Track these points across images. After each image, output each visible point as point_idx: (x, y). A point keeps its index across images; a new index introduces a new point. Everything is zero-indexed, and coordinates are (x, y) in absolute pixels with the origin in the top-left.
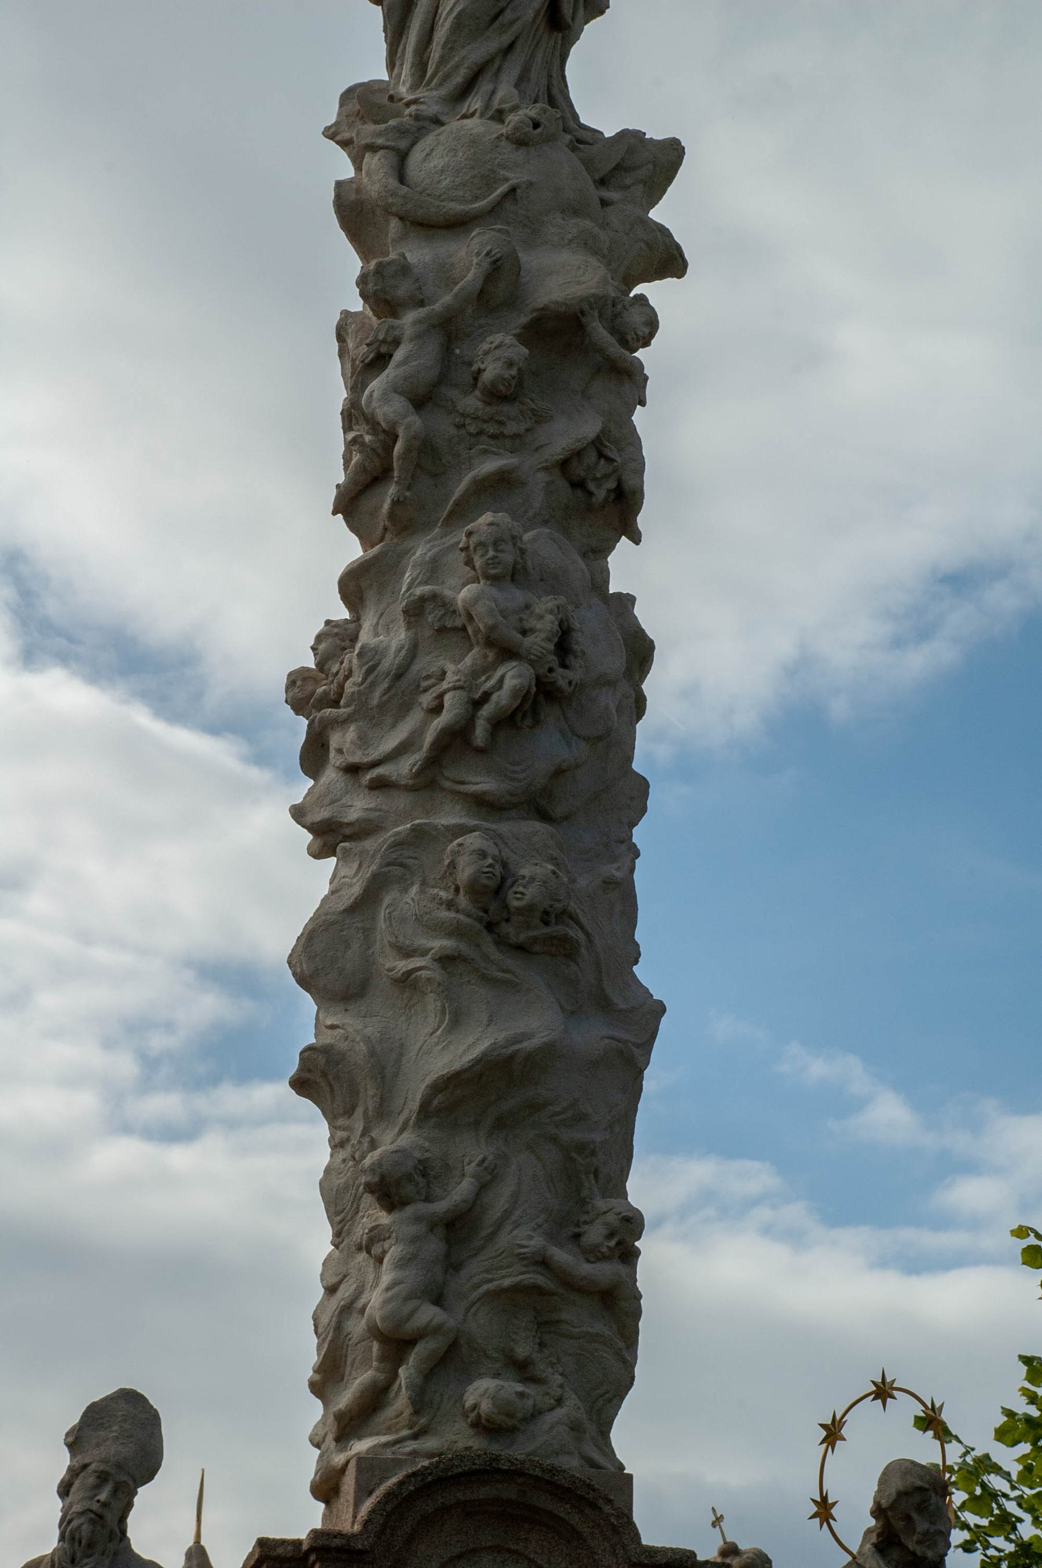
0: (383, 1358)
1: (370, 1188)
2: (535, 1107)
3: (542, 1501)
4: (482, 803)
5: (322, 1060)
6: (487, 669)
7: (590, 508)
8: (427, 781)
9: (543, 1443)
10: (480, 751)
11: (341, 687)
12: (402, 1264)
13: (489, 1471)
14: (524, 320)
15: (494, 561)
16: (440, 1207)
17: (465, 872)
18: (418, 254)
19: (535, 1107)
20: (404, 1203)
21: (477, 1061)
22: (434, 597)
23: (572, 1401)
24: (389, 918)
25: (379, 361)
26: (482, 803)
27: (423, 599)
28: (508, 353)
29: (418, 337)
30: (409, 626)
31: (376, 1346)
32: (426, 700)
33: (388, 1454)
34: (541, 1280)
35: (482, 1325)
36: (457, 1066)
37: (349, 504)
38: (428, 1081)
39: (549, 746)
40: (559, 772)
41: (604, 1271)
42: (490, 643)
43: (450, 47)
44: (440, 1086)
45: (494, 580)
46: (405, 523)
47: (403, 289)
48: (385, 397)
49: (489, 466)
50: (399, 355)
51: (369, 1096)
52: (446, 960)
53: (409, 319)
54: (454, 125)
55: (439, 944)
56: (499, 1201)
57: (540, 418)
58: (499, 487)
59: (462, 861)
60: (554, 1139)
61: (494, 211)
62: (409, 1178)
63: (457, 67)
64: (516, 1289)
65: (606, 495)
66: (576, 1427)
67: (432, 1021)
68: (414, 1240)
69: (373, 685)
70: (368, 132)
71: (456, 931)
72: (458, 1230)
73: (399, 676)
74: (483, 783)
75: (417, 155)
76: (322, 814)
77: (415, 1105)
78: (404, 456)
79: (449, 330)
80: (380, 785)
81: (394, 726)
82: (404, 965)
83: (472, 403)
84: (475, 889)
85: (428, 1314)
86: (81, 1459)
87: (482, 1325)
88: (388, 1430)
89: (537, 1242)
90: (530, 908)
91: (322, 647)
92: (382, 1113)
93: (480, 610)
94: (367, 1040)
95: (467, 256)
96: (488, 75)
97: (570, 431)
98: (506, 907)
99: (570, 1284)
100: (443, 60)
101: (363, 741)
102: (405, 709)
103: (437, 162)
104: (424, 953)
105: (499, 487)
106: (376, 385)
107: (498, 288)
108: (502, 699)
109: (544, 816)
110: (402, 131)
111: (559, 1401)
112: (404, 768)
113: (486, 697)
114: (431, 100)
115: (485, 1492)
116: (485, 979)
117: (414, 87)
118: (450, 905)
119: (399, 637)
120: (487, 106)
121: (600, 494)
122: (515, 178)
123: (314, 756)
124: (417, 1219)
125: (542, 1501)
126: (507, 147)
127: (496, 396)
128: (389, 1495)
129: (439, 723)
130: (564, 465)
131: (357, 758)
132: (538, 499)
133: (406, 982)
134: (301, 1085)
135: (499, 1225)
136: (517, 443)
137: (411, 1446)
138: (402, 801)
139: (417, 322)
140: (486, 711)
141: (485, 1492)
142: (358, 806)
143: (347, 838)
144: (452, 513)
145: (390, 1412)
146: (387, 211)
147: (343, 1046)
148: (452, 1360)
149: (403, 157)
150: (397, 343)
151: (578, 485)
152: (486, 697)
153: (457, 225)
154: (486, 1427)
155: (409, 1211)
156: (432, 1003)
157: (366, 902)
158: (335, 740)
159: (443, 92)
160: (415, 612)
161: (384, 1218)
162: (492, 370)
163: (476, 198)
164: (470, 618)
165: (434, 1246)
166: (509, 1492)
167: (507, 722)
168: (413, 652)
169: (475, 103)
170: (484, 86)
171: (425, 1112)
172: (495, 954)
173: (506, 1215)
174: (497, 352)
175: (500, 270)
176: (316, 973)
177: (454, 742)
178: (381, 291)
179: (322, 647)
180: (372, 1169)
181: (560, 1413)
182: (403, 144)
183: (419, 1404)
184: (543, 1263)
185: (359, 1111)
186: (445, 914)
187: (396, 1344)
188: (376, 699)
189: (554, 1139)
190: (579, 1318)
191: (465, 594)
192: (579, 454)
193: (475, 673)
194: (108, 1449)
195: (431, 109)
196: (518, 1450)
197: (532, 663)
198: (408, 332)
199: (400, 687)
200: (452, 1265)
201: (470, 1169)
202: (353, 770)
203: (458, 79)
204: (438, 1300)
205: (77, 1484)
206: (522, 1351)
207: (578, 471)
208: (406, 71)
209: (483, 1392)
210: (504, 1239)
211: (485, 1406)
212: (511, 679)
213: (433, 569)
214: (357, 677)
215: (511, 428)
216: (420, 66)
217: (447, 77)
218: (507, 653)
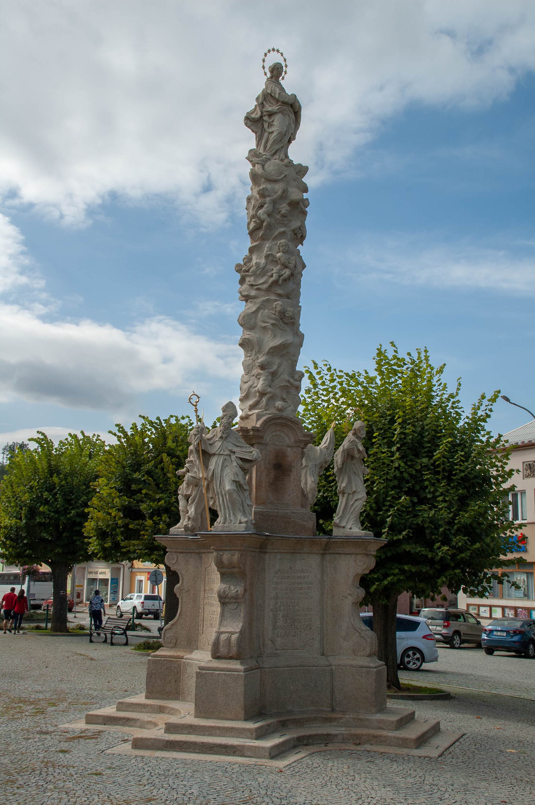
0: (259, 396)
1: (259, 366)
2: (288, 353)
3: (289, 423)
4: (280, 295)
5: (247, 341)
6: (282, 270)
7: (297, 239)
8: (269, 290)
9: (287, 413)
10: (279, 285)
11: (249, 269)
12: (264, 380)
13: (281, 418)
14: (288, 202)
15: (283, 249)
16: (272, 370)
17: (279, 308)
18: (269, 186)
19: (288, 353)
20: (265, 369)
21: (280, 344)
22: (271, 254)
23: (292, 406)
24: (261, 315)
25: (261, 207)
26: (280, 295)
27: (269, 254)
28: (287, 208)
29: (270, 203)
30: (265, 259)
31: (258, 394)
32: (269, 274)
33: (261, 413)
34: (288, 385)
35: (278, 392)
36: (275, 345)
37: (252, 233)
38: (269, 347)
39: (291, 285)
40: (293, 290)
41: (296, 383)
42: (283, 265)
43: (272, 145)
44: (271, 348)
45: (284, 252)
46: (264, 238)
47: (267, 193)
48: (263, 214)
49: (282, 230)
50: (266, 206)
51: (256, 349)
52: (273, 325)
53: (268, 199)
54: (273, 161)
55: (272, 321)
56: (281, 370)
57: (290, 221)
58: (282, 234)
59: (278, 306)
60: (290, 359)
61: (282, 179)
62: (266, 365)
63: (273, 149)
64: (284, 386)
65: (299, 236)
66: (293, 411)
67: (269, 336)
68: (267, 376)
69: (258, 270)
70: (255, 159)
71: (275, 319)
72: (274, 375)
73: (263, 269)
74: (280, 292)
75: (266, 166)
76: (246, 293)
77: (267, 351)
78: (265, 226)
79: (274, 202)
80: (258, 289)
81: (261, 278)
82: (264, 325)
83: (278, 217)
84: (280, 312)
85: (269, 390)
86: (225, 414)
87: (278, 392)
88: (260, 409)
89: (288, 378)
90: (290, 316)
91: (245, 260)
92: (259, 352)
93: (283, 258)
94: (256, 338)
95: (279, 187)
96: (279, 151)
97: (295, 224)
98: (285, 315)
99: (292, 385)
100: (270, 148)
101: (255, 280)
102: (264, 275)
103: (271, 168)
104: (268, 323)
105: (282, 234)
106: (261, 211)
107: (284, 195)
108: (285, 276)
109: (288, 298)
110: (263, 160)
111: (290, 406)
112: (265, 286)
113: (282, 275)
114: (268, 154)
115: (279, 421)
116: (280, 329)
117: (264, 151)
118: (274, 314)
119: (263, 261)
120: (279, 158)
121: (299, 237)
122: (286, 173)
123: (242, 281)
124: (268, 372)
125: (289, 423)
126: (284, 167)
127: (283, 216)
128: (265, 421)
129: (271, 280)
130: (293, 230)
131: (254, 283)
132: (289, 237)
133: (265, 328)
134: (241, 345)
135: (281, 374)
136: (286, 225)
137: (265, 412)
138: (262, 293)
139: (270, 200)
140: (282, 278)
141: (279, 421)
142: (253, 293)
143: (251, 298)
144: (274, 238)
145: (260, 406)
146: (262, 177)
147: (251, 338)
148: (273, 398)
149: (263, 166)
150: (265, 203)
151: (295, 234)
152: (282, 275)
153: (275, 181)
154: (280, 410)
155: (266, 371)
156: (270, 332)
157: (256, 312)
158: (248, 279)
159: (270, 153)
160: (267, 257)
161: (260, 371)
162: (283, 211)
163: (279, 176)
164: (280, 259)
165: (270, 377)
166: (283, 421)
167: (285, 280)
168: (266, 264)
169: (277, 157)
170: (278, 153)
171: (268, 353)
172: (282, 323)
173: (283, 372)
174: (284, 208)
175: (285, 191)
176: (245, 324)
177: (276, 282)
178: (263, 194)
179: (245, 260)
180: (260, 363)
181: (290, 408)
182: (263, 163)
183: (267, 405)
184: (289, 382)
185: (254, 351)
186: (273, 316)
187: (262, 394)
188: (258, 272)
189: (290, 359)
190: (293, 391)
191: (279, 255)
192: (296, 229)
193: (279, 270)
194: (229, 413)
195: (269, 157)
196: (285, 414)
197: (291, 269)
198: (268, 202)
199: (262, 271)
200: (272, 381)
201: (277, 364)
202: (252, 285)
203: (274, 151)
204: (270, 387)
205: (225, 418)
206: (284, 397)
207: (296, 232)
208: (262, 148)
209: (279, 404)
210: (282, 377)
211: (280, 406)
212: (287, 272)
213: (270, 249)
214: (254, 268)
215: (285, 222)
216: (265, 147)
217: (271, 151)
218: (286, 267)
